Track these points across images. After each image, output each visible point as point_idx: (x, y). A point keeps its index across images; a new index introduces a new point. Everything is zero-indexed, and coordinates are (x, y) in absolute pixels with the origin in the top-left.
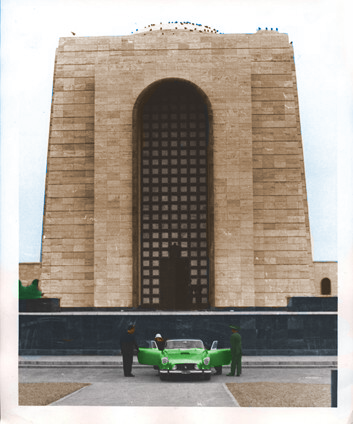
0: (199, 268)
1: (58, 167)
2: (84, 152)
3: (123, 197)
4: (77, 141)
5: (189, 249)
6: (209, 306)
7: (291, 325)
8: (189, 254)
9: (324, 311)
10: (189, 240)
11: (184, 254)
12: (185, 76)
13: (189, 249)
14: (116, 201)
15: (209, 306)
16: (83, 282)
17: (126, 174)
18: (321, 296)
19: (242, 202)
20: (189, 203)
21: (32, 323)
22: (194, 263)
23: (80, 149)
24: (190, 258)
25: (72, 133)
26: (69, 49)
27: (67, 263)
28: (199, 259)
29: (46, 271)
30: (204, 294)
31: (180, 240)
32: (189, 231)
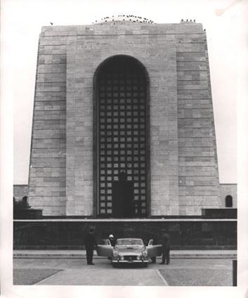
1: (41, 118)
2: (59, 107)
3: (86, 139)
4: (55, 99)
5: (132, 175)
6: (147, 215)
8: (109, 182)
10: (133, 169)
13: (132, 175)
15: (147, 215)
17: (88, 122)
21: (23, 227)
22: (136, 185)
24: (134, 181)
27: (47, 184)
28: (140, 182)
29: (32, 191)
30: (143, 207)
31: (126, 168)
32: (133, 162)
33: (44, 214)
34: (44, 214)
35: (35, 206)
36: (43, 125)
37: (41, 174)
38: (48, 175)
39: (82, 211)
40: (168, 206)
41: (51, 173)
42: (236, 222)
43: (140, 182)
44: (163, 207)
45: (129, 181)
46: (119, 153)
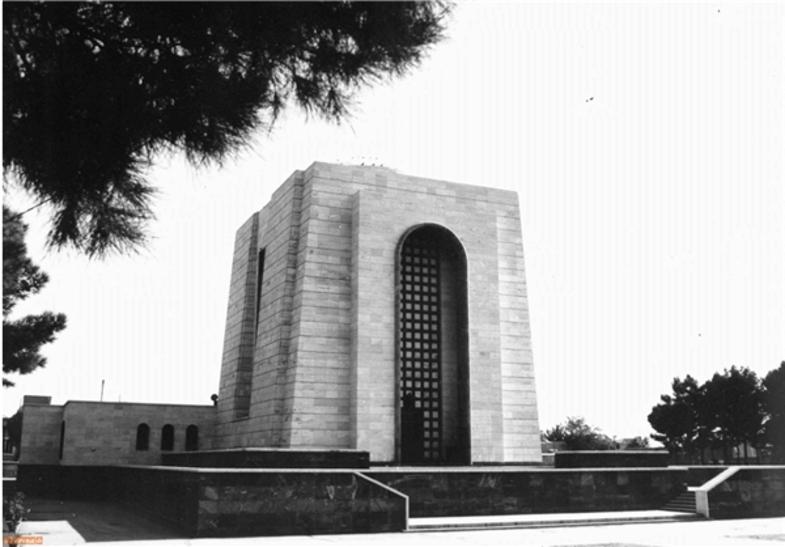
0: (431, 420)
1: (311, 302)
2: (337, 288)
3: (385, 342)
4: (331, 276)
5: (422, 400)
6: (466, 461)
7: (621, 481)
8: (422, 404)
9: (179, 465)
10: (422, 390)
11: (418, 404)
12: (441, 222)
13: (422, 400)
14: (379, 345)
15: (466, 461)
16: (335, 432)
17: (388, 318)
18: (185, 452)
19: (492, 355)
20: (422, 351)
21: (399, 481)
22: (426, 414)
23: (336, 285)
24: (423, 409)
25: (327, 266)
26: (508, 202)
27: (319, 410)
28: (431, 410)
29: (298, 419)
30: (459, 448)
31: (414, 389)
32: (422, 380)
33: (373, 458)
34: (373, 458)
35: (303, 445)
36: (314, 313)
37: (311, 393)
38: (321, 395)
39: (380, 454)
40: (490, 447)
41: (325, 391)
42: (4, 476)
43: (431, 410)
44: (485, 450)
45: (418, 409)
46: (409, 369)
